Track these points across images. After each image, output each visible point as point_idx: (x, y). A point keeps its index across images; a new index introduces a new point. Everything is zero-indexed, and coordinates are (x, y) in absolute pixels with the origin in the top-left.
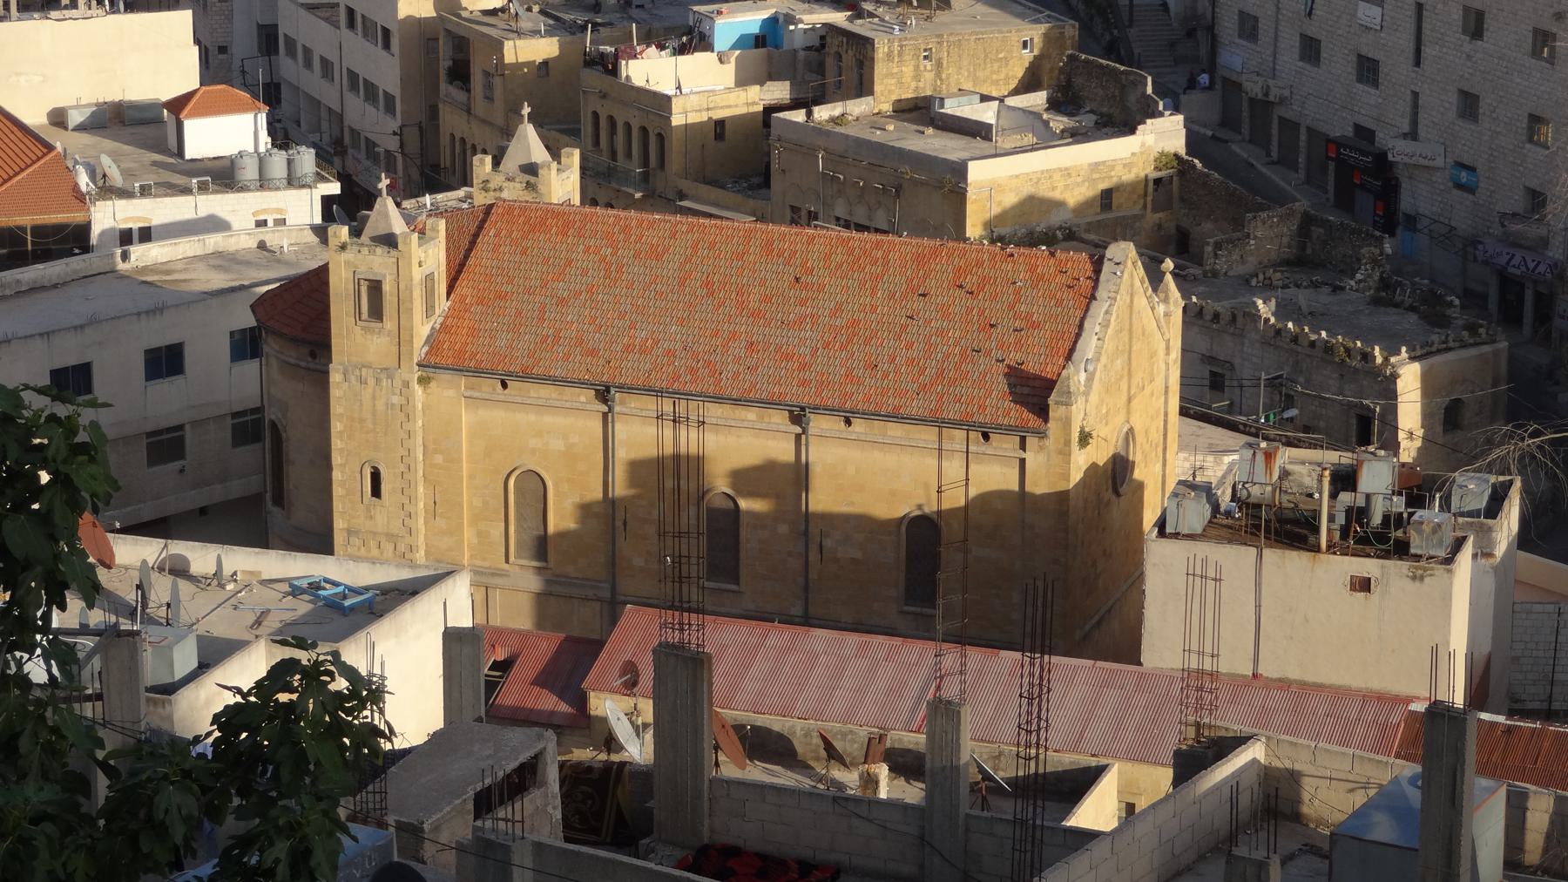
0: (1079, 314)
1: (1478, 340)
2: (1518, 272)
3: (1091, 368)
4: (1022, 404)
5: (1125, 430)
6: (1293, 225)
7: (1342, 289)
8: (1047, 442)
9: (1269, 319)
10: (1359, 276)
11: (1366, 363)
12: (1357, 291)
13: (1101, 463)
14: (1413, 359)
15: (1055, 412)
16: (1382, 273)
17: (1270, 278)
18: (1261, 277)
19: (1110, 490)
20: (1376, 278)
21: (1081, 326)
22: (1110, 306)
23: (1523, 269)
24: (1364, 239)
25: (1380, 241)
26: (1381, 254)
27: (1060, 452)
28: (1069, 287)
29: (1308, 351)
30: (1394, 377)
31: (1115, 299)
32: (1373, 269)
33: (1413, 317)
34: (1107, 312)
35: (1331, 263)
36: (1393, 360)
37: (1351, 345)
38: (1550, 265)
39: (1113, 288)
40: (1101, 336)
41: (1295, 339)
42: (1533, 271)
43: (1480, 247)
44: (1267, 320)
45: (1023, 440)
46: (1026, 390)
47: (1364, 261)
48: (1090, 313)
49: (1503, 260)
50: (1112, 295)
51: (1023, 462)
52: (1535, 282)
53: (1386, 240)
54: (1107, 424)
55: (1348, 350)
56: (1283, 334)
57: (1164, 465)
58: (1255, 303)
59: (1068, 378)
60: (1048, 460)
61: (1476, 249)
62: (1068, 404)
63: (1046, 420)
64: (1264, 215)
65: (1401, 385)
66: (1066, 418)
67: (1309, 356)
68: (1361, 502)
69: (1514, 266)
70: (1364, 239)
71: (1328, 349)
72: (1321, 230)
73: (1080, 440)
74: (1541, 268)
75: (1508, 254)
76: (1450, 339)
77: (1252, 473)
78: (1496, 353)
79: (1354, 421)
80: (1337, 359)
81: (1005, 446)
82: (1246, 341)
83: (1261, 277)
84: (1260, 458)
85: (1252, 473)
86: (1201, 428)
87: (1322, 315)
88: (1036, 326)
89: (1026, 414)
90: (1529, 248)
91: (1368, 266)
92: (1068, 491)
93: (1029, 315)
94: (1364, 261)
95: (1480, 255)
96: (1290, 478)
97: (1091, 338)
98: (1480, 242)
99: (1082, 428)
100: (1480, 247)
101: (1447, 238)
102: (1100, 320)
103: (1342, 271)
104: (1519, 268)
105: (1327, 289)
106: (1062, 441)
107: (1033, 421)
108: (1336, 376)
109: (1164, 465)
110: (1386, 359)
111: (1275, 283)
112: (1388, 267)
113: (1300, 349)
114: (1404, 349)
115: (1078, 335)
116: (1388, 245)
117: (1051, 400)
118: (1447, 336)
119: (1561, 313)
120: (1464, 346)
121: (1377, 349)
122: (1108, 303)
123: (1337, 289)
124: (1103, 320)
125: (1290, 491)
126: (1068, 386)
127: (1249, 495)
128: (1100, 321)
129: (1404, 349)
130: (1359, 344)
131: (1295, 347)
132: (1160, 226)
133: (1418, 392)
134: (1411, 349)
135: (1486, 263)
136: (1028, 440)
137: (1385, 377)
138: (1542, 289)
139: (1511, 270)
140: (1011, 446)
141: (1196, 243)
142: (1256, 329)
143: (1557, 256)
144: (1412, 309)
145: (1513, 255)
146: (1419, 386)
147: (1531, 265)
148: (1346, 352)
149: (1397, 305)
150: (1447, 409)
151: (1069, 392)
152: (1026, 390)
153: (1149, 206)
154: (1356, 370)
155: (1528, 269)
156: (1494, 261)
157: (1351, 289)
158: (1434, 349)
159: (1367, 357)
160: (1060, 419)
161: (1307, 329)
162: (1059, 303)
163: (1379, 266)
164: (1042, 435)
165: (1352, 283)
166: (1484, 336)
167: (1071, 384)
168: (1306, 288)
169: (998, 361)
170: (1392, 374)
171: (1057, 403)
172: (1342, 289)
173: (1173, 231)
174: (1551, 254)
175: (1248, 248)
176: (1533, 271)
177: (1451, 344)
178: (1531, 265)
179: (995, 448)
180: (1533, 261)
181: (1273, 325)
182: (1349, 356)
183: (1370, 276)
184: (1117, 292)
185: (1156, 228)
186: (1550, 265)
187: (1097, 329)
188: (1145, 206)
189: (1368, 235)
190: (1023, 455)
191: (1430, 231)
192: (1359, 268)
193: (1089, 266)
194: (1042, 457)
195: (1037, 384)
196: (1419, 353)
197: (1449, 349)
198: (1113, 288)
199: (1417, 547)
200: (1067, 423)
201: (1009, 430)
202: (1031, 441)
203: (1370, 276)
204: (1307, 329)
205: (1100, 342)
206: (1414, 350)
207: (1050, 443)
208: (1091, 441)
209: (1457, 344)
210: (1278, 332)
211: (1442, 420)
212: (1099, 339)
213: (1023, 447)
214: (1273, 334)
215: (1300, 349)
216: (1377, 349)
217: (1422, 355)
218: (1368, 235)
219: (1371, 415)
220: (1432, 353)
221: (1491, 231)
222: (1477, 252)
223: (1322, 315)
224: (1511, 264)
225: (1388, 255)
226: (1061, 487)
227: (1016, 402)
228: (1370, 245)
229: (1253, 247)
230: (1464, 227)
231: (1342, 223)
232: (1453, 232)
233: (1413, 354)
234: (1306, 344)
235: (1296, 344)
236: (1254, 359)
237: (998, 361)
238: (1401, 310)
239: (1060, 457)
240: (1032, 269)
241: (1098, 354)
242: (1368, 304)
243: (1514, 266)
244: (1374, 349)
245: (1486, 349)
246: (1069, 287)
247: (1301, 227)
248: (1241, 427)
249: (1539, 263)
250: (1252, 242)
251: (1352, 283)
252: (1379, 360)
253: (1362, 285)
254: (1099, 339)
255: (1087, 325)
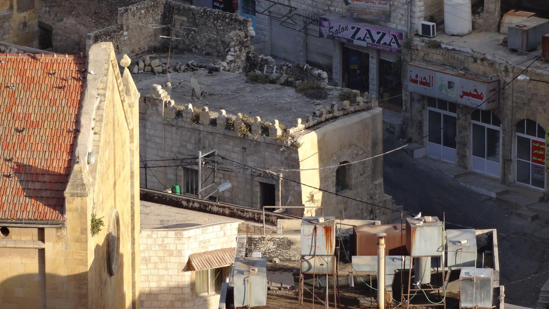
0: (73, 111)
1: (358, 108)
2: (364, 44)
3: (93, 160)
4: (37, 198)
5: (114, 215)
6: (158, 15)
7: (217, 70)
8: (64, 232)
9: (169, 102)
10: (229, 58)
11: (268, 135)
12: (229, 71)
13: (101, 244)
14: (309, 128)
15: (71, 204)
16: (248, 53)
17: (150, 65)
18: (142, 65)
19: (106, 272)
20: (243, 58)
21: (77, 122)
22: (101, 102)
23: (369, 41)
24: (228, 24)
25: (244, 23)
26: (246, 37)
27: (78, 240)
28: (60, 88)
29: (210, 129)
30: (295, 147)
31: (104, 95)
32: (240, 50)
33: (290, 91)
34: (98, 108)
35: (196, 47)
36: (292, 131)
37: (251, 121)
38: (394, 36)
39: (101, 86)
40: (96, 130)
41: (196, 119)
42: (379, 41)
43: (326, 24)
44: (167, 104)
45: (41, 232)
46: (37, 186)
47: (233, 43)
48: (84, 110)
49: (348, 34)
50: (101, 92)
51: (42, 252)
52: (379, 51)
53: (250, 24)
54: (103, 210)
55: (249, 126)
56: (184, 115)
57: (133, 243)
58: (155, 89)
59: (81, 171)
60: (66, 248)
61: (321, 25)
62: (83, 195)
63: (62, 211)
64: (133, 8)
65: (302, 153)
66: (82, 208)
67: (212, 133)
68: (409, 266)
69: (359, 39)
70: (228, 24)
71: (229, 125)
72: (185, 19)
73: (93, 228)
74: (387, 39)
75: (353, 28)
76: (335, 108)
77: (314, 246)
78: (373, 118)
79: (258, 189)
80: (239, 135)
81: (24, 238)
82: (148, 124)
83: (142, 65)
84: (321, 232)
85: (314, 246)
86: (146, 207)
87: (210, 95)
88: (37, 125)
89: (42, 208)
90: (372, 22)
91: (236, 48)
92: (86, 273)
93: (27, 116)
94: (233, 43)
95: (325, 31)
96: (293, 247)
97: (89, 132)
98: (325, 20)
99: (93, 216)
100: (326, 24)
101: (289, 18)
102: (93, 116)
103: (208, 54)
104: (364, 40)
105: (202, 71)
106: (79, 229)
107: (51, 213)
108: (237, 149)
109: (133, 243)
110: (285, 131)
111: (156, 69)
112: (252, 48)
113: (201, 128)
114: (300, 121)
115: (77, 131)
116: (252, 28)
117: (67, 193)
118: (333, 106)
119: (414, 77)
120: (347, 114)
121: (277, 122)
122: (99, 100)
123: (213, 71)
124: (96, 115)
125: (293, 259)
126: (82, 179)
127: (310, 267)
128: (93, 116)
129: (300, 121)
130: (259, 119)
131: (197, 126)
132: (25, 24)
133: (316, 158)
134: (306, 120)
135: (332, 37)
136: (47, 232)
137: (287, 148)
138: (391, 59)
139: (356, 42)
140: (30, 238)
141: (59, 38)
142: (158, 113)
143: (400, 27)
144: (287, 84)
145: (358, 29)
146: (317, 151)
147: (376, 37)
148: (247, 127)
149: (273, 82)
150: (337, 170)
151: (83, 185)
152: (37, 186)
153: (15, 7)
154: (258, 143)
155: (373, 41)
156: (339, 35)
157: (224, 70)
158: (323, 119)
159: (266, 130)
160: (76, 210)
161: (207, 109)
162: (53, 103)
163: (245, 47)
164: (60, 225)
165: (225, 64)
166: (362, 104)
167: (84, 177)
168: (184, 71)
169: (6, 160)
170: (292, 145)
171: (72, 195)
172: (217, 70)
173: (36, 28)
174: (393, 26)
175: (122, 39)
176: (379, 41)
177: (336, 113)
178: (376, 37)
179: (15, 241)
180: (378, 33)
181: (174, 107)
182: (250, 130)
183: (238, 57)
184: (105, 89)
185: (21, 26)
186: (394, 36)
187: (93, 124)
188: (11, 7)
189: (231, 20)
190: (42, 245)
191: (270, 12)
192: (229, 50)
193: (74, 67)
194: (60, 246)
195: (47, 178)
196: (311, 123)
197: (335, 118)
198: (101, 86)
199: (466, 301)
200: (83, 212)
201: (28, 223)
202: (49, 232)
203: (238, 57)
204: (207, 109)
205: (97, 136)
206: (307, 121)
207: (68, 232)
208: (101, 227)
209: (341, 113)
210: (179, 114)
211: (335, 182)
212: (95, 133)
213: (42, 238)
214: (174, 116)
215: (201, 128)
216: (277, 122)
217: (314, 125)
218: (231, 20)
219: (274, 183)
220: (322, 122)
221: (332, 9)
222: (323, 29)
223: (210, 95)
224: (357, 37)
225: (252, 37)
226: (80, 270)
227: (30, 197)
228: (235, 29)
229: (126, 38)
230: (304, 6)
231: (205, 12)
232: (293, 13)
233: (307, 125)
234: (208, 122)
235: (198, 123)
236: (158, 140)
237: (6, 160)
238: (278, 86)
239: (78, 245)
240: (22, 73)
241: (97, 146)
242: (247, 82)
243: (359, 39)
244: (274, 123)
245: (365, 115)
246: (60, 88)
247: (164, 16)
248: (184, 203)
249: (384, 35)
250: (125, 33)
251: (225, 64)
252: (279, 132)
253: (232, 65)
254: (95, 133)
255: (83, 120)
